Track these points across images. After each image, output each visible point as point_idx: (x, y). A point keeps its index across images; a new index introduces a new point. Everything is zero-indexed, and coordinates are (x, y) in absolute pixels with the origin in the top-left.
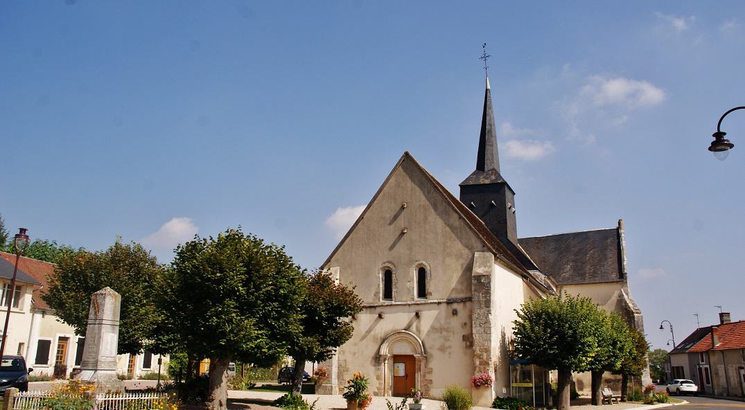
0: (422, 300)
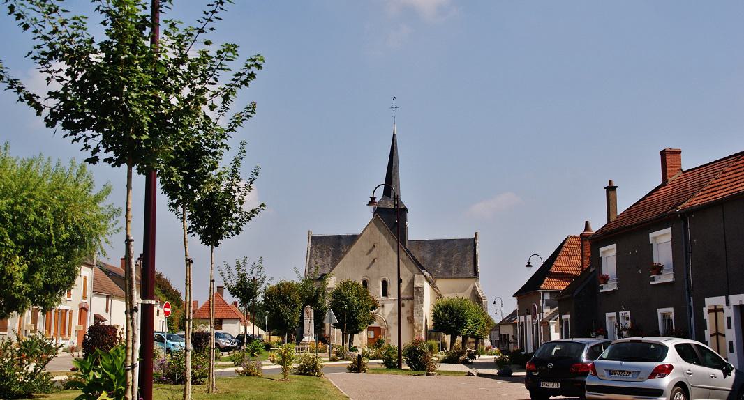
0: (385, 298)
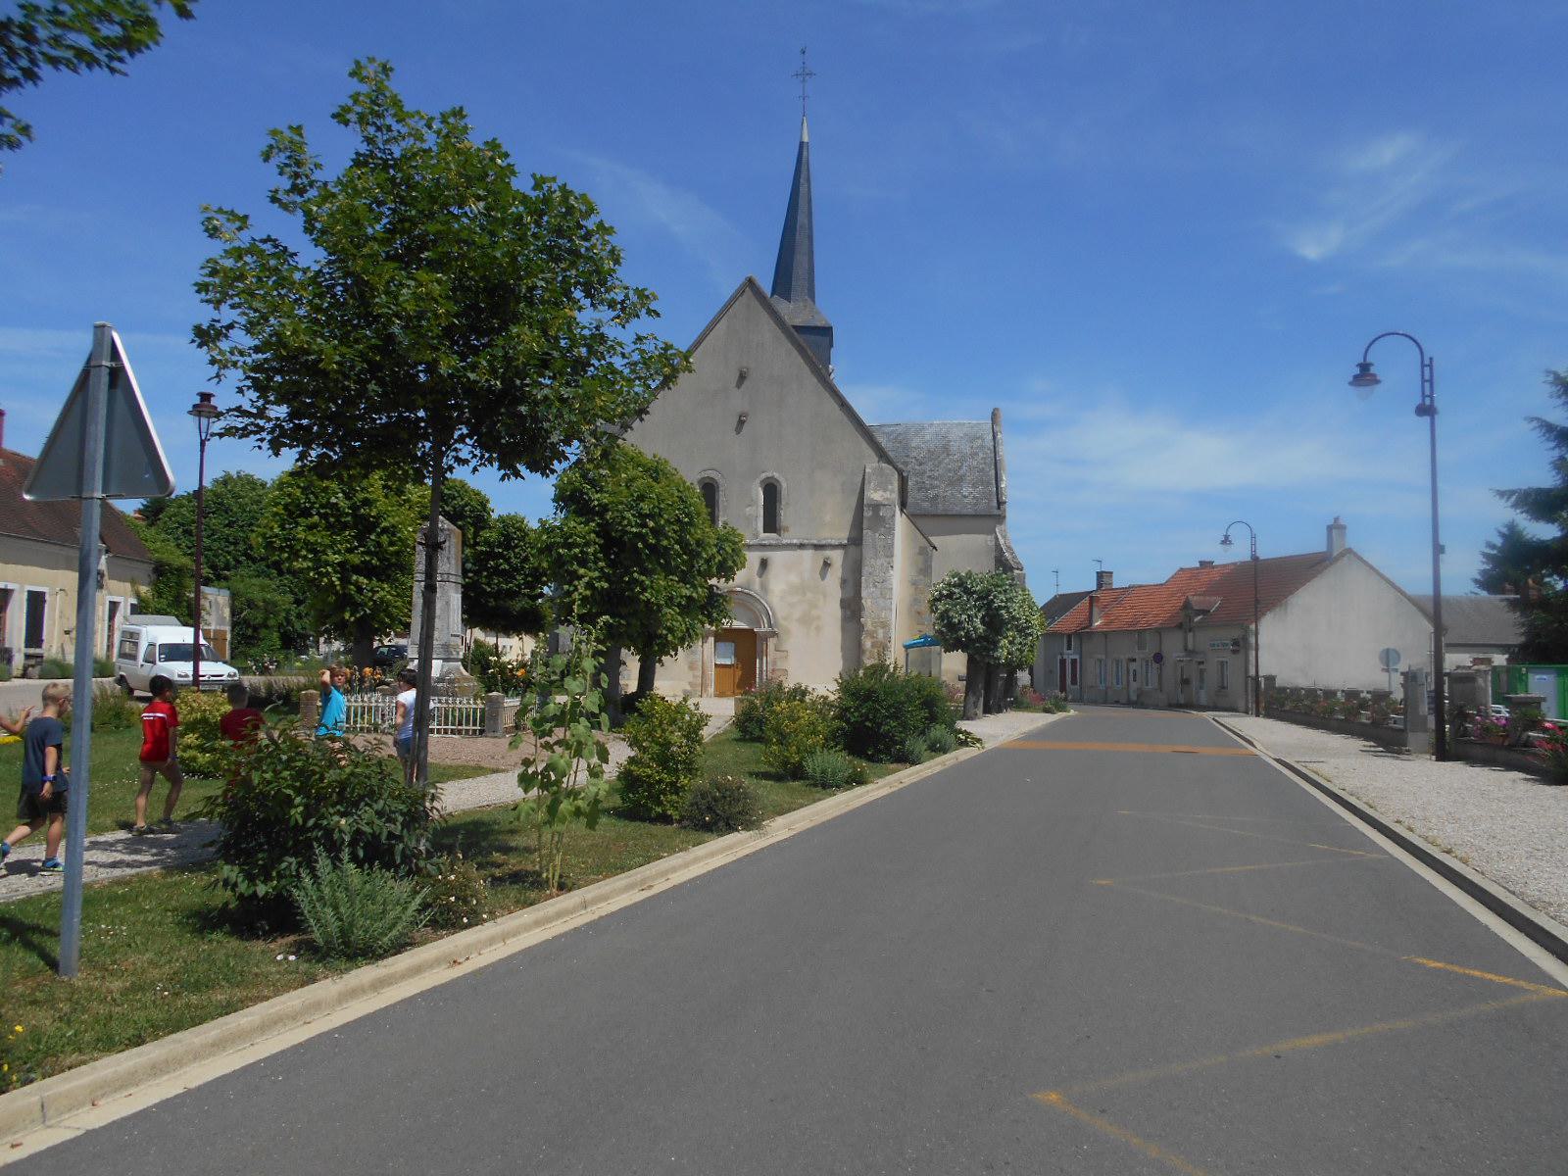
0: (771, 538)
